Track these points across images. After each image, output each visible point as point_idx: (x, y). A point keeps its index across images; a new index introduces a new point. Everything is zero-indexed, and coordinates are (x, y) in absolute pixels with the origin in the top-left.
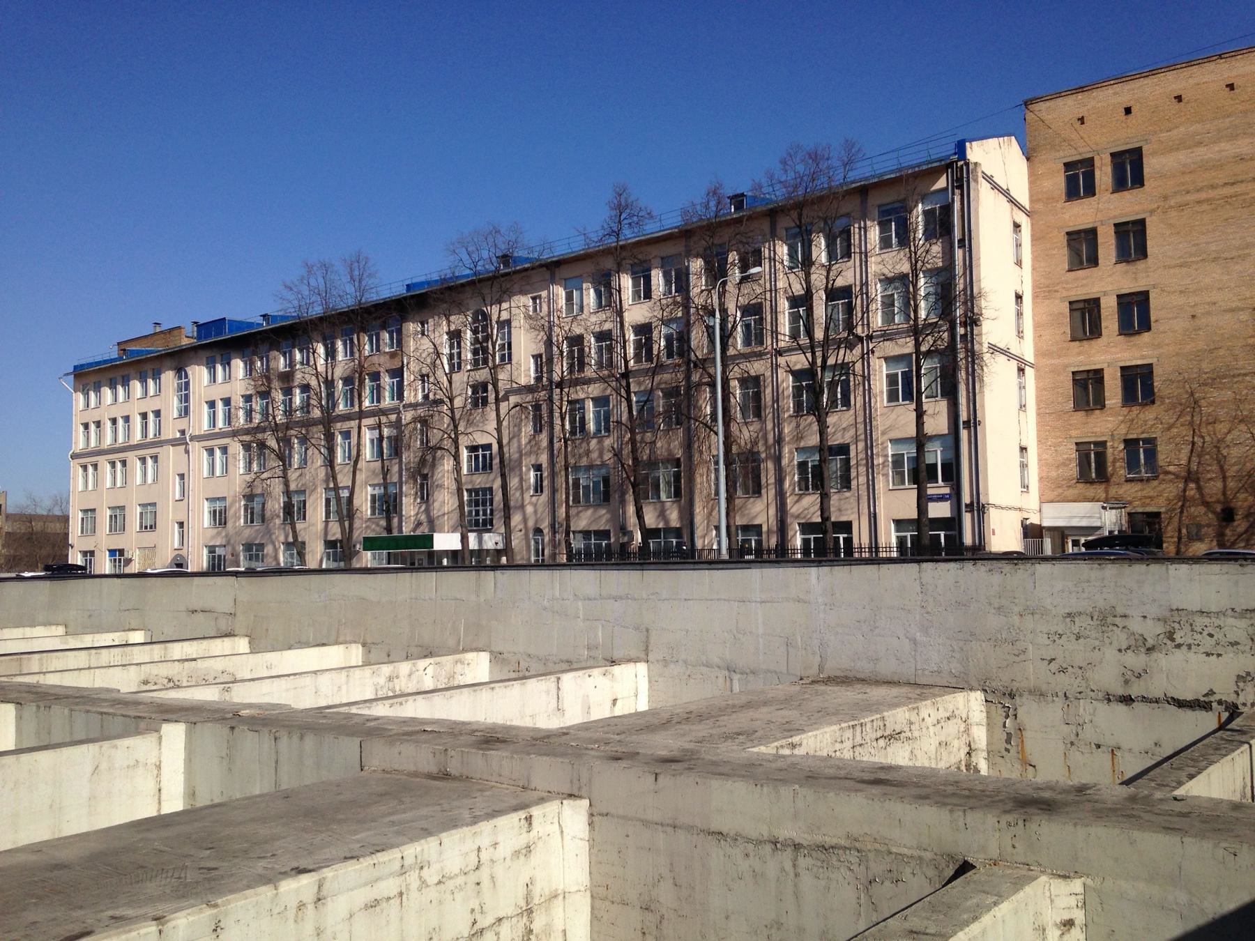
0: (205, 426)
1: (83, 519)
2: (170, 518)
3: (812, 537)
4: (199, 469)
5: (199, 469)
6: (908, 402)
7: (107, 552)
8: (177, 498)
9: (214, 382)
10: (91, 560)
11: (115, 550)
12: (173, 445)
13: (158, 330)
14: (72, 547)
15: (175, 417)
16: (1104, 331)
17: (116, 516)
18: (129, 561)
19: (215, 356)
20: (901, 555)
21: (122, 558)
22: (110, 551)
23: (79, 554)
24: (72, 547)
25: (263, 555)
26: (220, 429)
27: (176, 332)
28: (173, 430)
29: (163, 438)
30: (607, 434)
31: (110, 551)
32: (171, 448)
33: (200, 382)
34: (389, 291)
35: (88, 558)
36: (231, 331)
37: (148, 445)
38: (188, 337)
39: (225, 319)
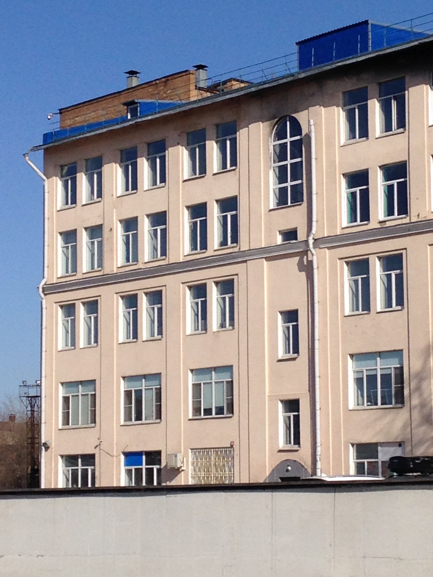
0: (60, 271)
1: (66, 400)
2: (267, 394)
3: (366, 461)
4: (334, 299)
5: (334, 299)
6: (366, 312)
7: (122, 457)
8: (281, 354)
9: (74, 201)
10: (85, 473)
11: (139, 454)
12: (268, 259)
13: (135, 82)
14: (47, 448)
15: (272, 207)
16: (301, 273)
17: (139, 393)
18: (176, 471)
19: (404, 78)
20: (137, 485)
21: (155, 468)
22: (127, 455)
23: (60, 459)
24: (47, 448)
25: (159, 470)
26: (380, 222)
27: (178, 81)
28: (269, 230)
29: (244, 245)
30: (399, 308)
31: (127, 455)
32: (265, 263)
33: (331, 138)
34: (284, 67)
35: (80, 467)
36: (377, 44)
37: (214, 261)
38: (200, 89)
39: (366, 22)
